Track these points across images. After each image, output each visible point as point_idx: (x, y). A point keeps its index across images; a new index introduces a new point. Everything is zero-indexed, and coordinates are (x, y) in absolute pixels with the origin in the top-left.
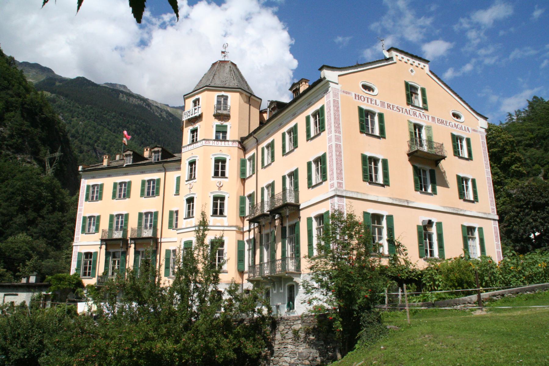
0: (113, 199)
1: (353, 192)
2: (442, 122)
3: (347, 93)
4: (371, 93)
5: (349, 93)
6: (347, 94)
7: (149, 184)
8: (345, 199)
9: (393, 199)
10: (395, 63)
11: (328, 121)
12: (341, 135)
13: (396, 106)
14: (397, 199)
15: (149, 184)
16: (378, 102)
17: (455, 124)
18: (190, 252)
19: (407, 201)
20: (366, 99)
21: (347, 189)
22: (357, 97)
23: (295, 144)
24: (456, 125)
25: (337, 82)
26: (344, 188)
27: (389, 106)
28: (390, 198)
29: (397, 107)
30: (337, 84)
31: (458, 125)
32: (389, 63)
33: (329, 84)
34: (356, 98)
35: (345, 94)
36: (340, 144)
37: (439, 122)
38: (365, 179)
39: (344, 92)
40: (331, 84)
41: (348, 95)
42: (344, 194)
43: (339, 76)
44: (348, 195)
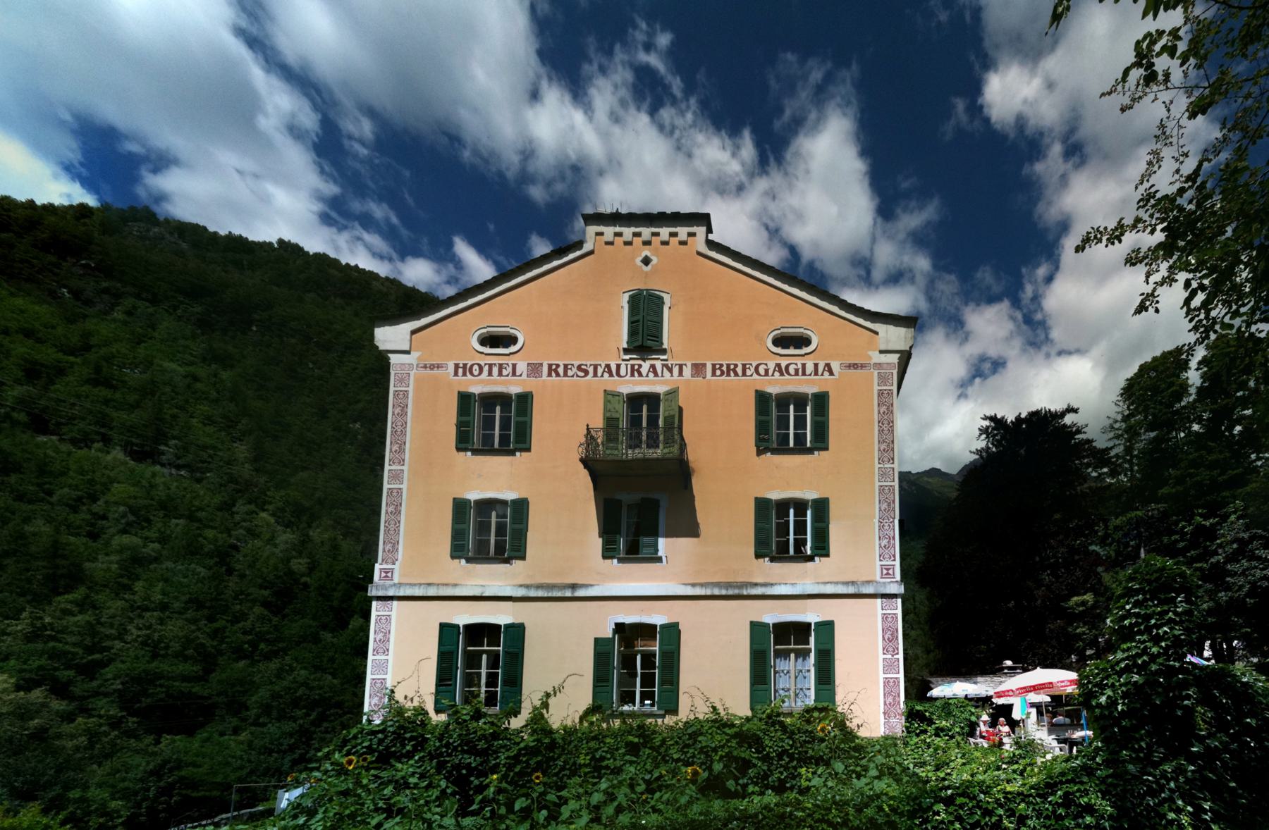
0: (605, 557)
1: (415, 585)
2: (731, 370)
3: (432, 367)
4: (513, 349)
5: (439, 366)
6: (432, 369)
7: (800, 439)
8: (395, 603)
9: (527, 587)
10: (591, 253)
11: (394, 432)
12: (405, 468)
13: (577, 363)
14: (539, 587)
15: (800, 439)
16: (522, 367)
17: (778, 365)
18: (170, 747)
19: (574, 587)
20: (486, 369)
21: (402, 581)
22: (460, 371)
23: (1144, 231)
24: (783, 366)
25: (406, 348)
26: (396, 580)
27: (552, 370)
28: (521, 586)
29: (579, 368)
30: (408, 352)
31: (787, 367)
32: (565, 259)
33: (389, 358)
34: (456, 374)
35: (428, 371)
36: (401, 486)
37: (718, 372)
38: (454, 554)
39: (425, 367)
40: (394, 359)
41: (435, 372)
42: (391, 593)
43: (414, 332)
44: (401, 594)
